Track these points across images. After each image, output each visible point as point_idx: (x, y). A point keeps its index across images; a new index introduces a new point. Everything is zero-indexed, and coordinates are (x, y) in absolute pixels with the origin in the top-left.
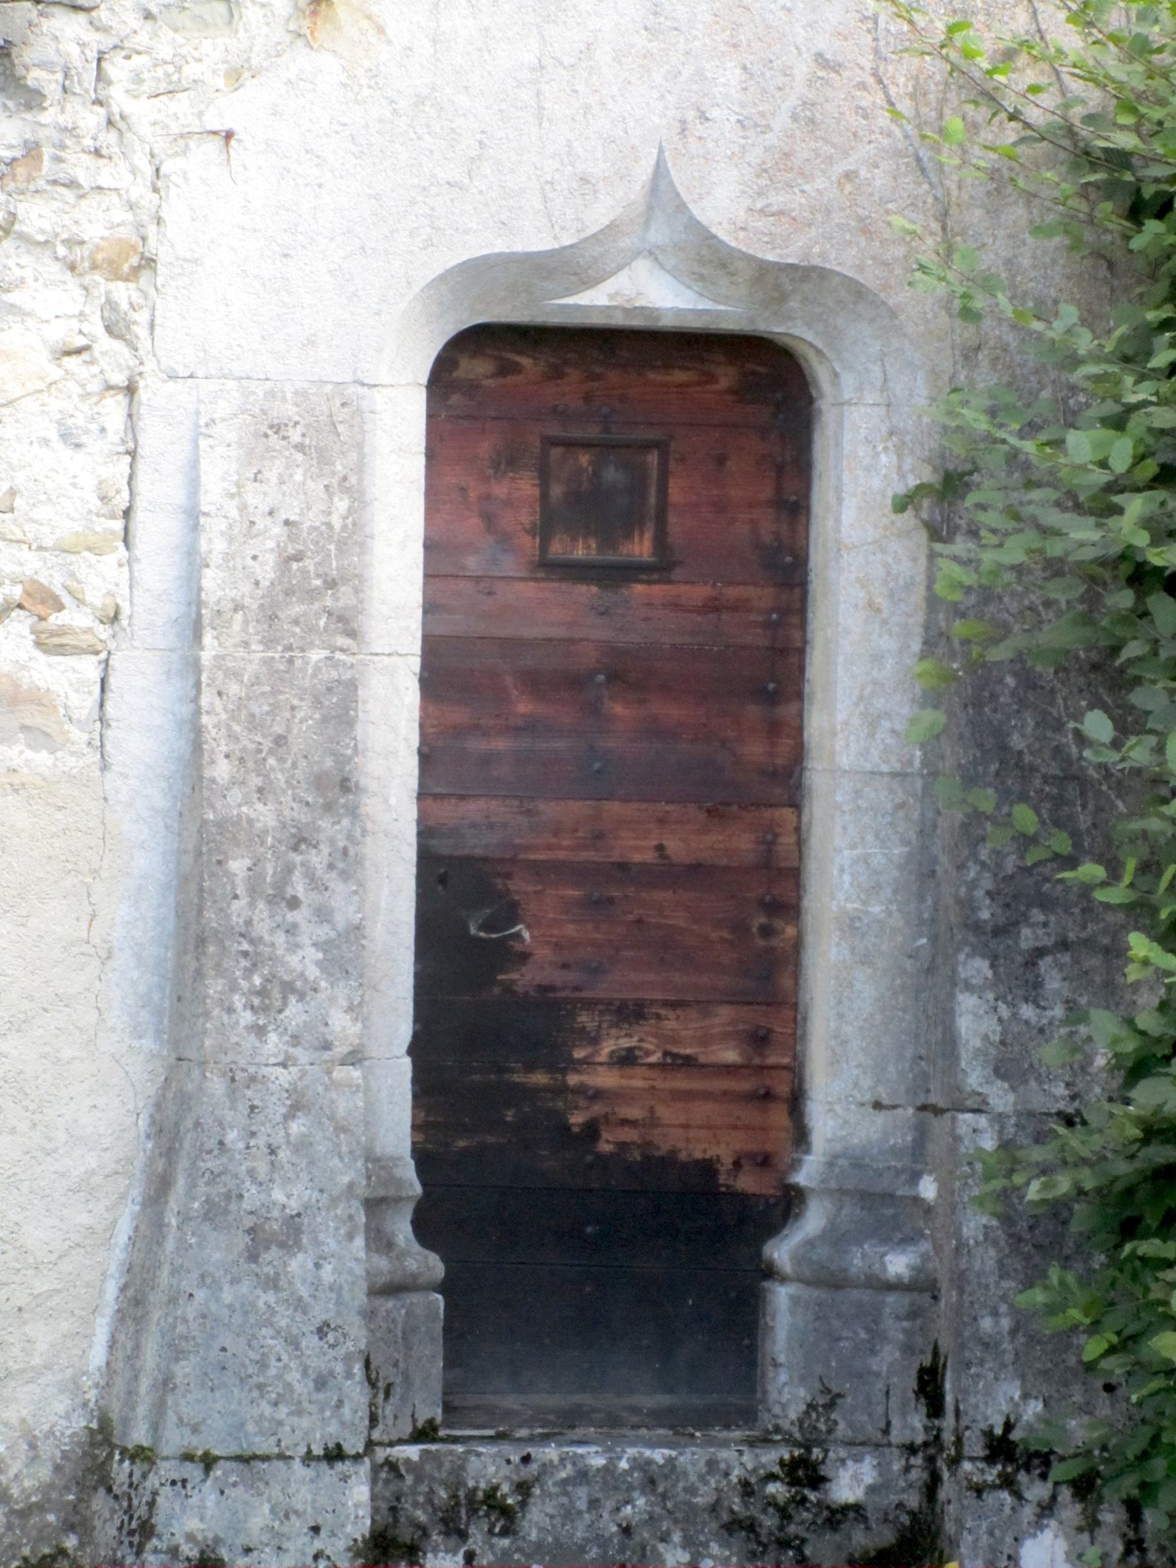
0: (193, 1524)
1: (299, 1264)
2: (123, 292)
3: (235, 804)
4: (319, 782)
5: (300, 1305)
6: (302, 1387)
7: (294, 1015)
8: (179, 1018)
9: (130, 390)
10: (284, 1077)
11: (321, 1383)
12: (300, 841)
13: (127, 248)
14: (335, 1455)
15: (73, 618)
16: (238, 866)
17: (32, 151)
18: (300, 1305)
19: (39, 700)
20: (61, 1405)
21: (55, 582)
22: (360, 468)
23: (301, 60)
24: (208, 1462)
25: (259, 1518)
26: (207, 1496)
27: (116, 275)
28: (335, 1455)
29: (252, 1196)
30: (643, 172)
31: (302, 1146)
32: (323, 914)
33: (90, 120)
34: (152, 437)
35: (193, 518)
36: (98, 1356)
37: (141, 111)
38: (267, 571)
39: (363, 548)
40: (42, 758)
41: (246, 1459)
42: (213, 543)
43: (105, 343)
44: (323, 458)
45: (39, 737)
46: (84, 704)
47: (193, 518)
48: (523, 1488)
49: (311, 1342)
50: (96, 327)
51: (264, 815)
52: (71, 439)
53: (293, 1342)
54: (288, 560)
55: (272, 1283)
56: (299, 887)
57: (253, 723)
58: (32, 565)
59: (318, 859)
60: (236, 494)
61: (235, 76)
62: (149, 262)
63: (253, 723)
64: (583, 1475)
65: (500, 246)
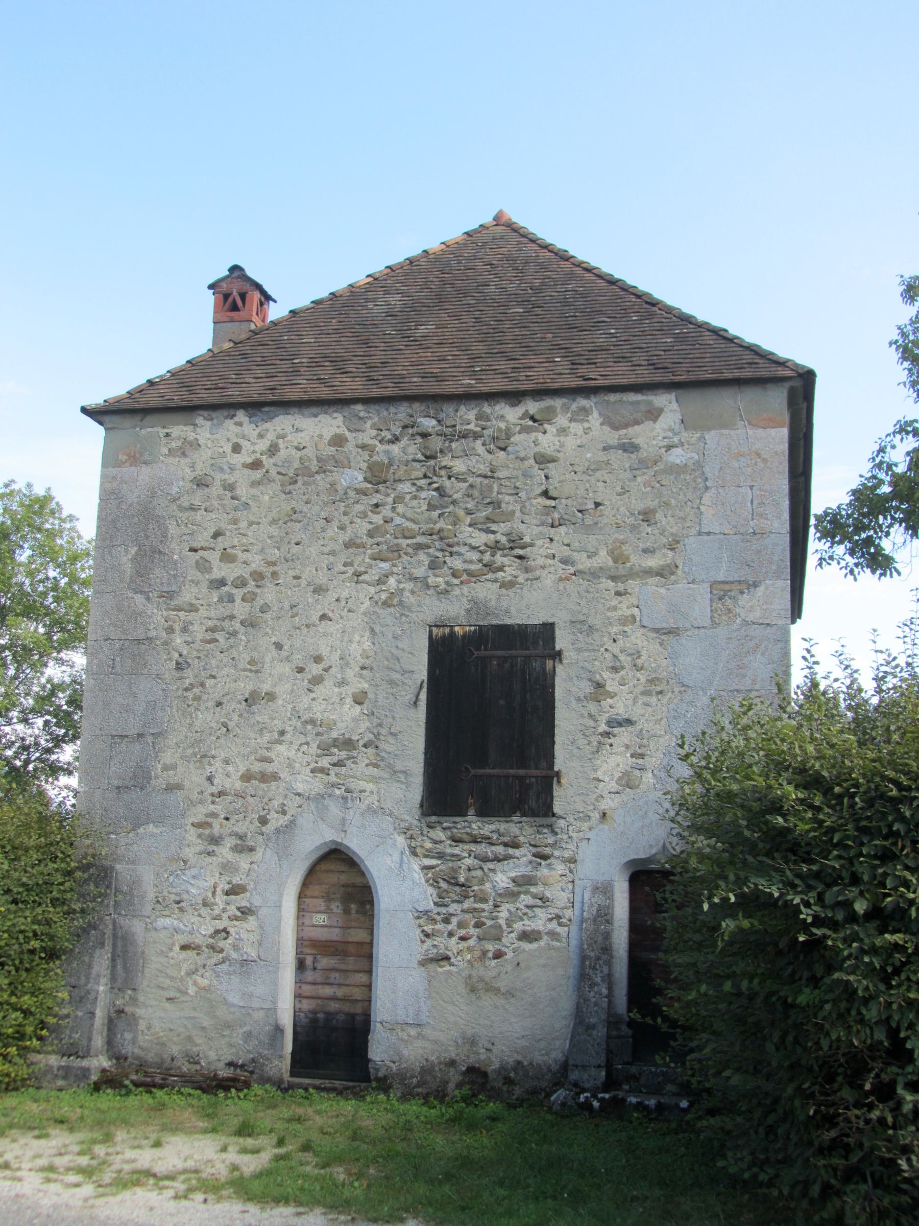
0: (574, 1077)
1: (594, 1032)
2: (572, 866)
3: (588, 952)
4: (602, 949)
5: (594, 1039)
6: (594, 1054)
7: (596, 988)
8: (109, 1030)
9: (573, 882)
10: (594, 1000)
11: (597, 1054)
12: (598, 959)
13: (572, 858)
14: (599, 1066)
15: (564, 920)
16: (587, 963)
17: (556, 842)
18: (594, 1039)
19: (558, 934)
20: (561, 1055)
21: (561, 914)
22: (612, 895)
23: (601, 826)
24: (577, 1066)
25: (586, 1077)
26: (577, 1072)
27: (570, 863)
28: (599, 1066)
29: (587, 1020)
30: (661, 844)
31: (596, 1012)
32: (602, 972)
33: (565, 837)
34: (577, 890)
35: (583, 903)
36: (567, 1046)
37: (574, 835)
38: (594, 912)
39: (613, 908)
40: (558, 944)
41: (583, 1066)
42: (586, 908)
43: (569, 874)
44: (605, 893)
45: (558, 940)
46: (565, 935)
47: (583, 903)
48: (640, 1074)
49: (596, 1046)
50: (567, 871)
51: (592, 954)
52: (563, 890)
53: (593, 1046)
54: (598, 911)
55: (590, 1036)
56: (598, 967)
57: (591, 939)
58: (557, 911)
59: (601, 962)
60: (590, 899)
61: (590, 829)
62: (576, 861)
63: (591, 939)
64: (651, 1072)
65: (636, 857)
